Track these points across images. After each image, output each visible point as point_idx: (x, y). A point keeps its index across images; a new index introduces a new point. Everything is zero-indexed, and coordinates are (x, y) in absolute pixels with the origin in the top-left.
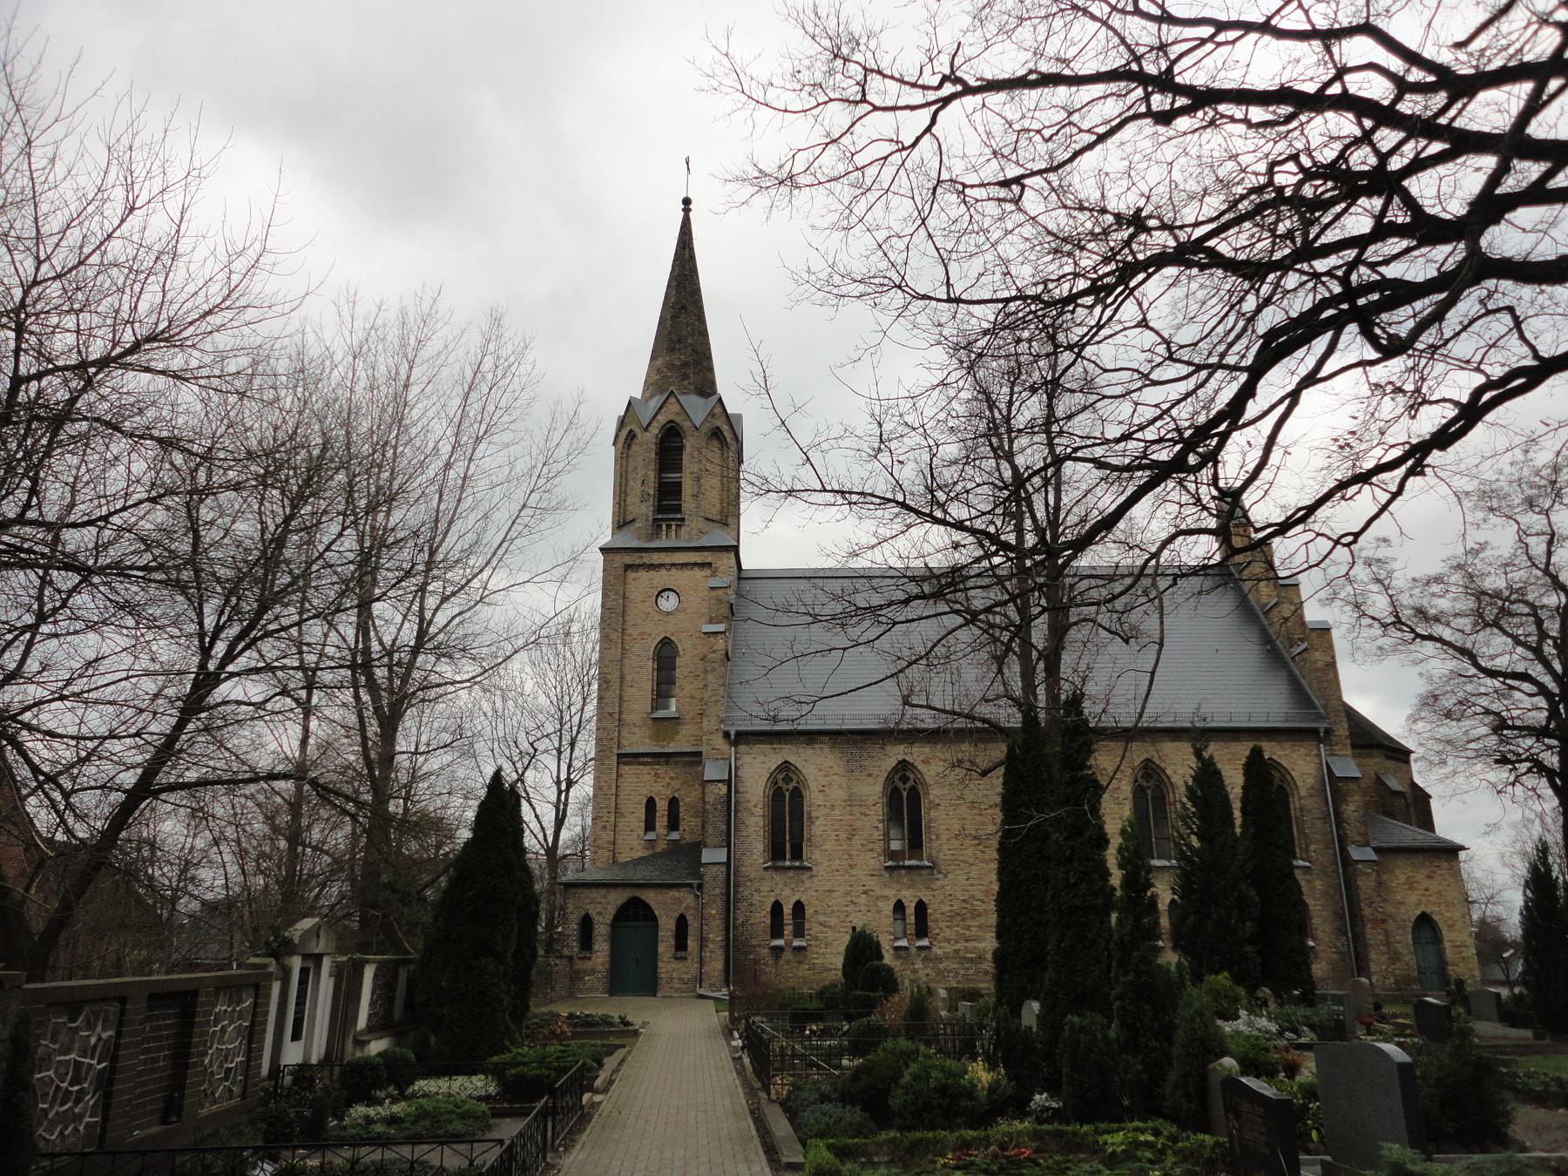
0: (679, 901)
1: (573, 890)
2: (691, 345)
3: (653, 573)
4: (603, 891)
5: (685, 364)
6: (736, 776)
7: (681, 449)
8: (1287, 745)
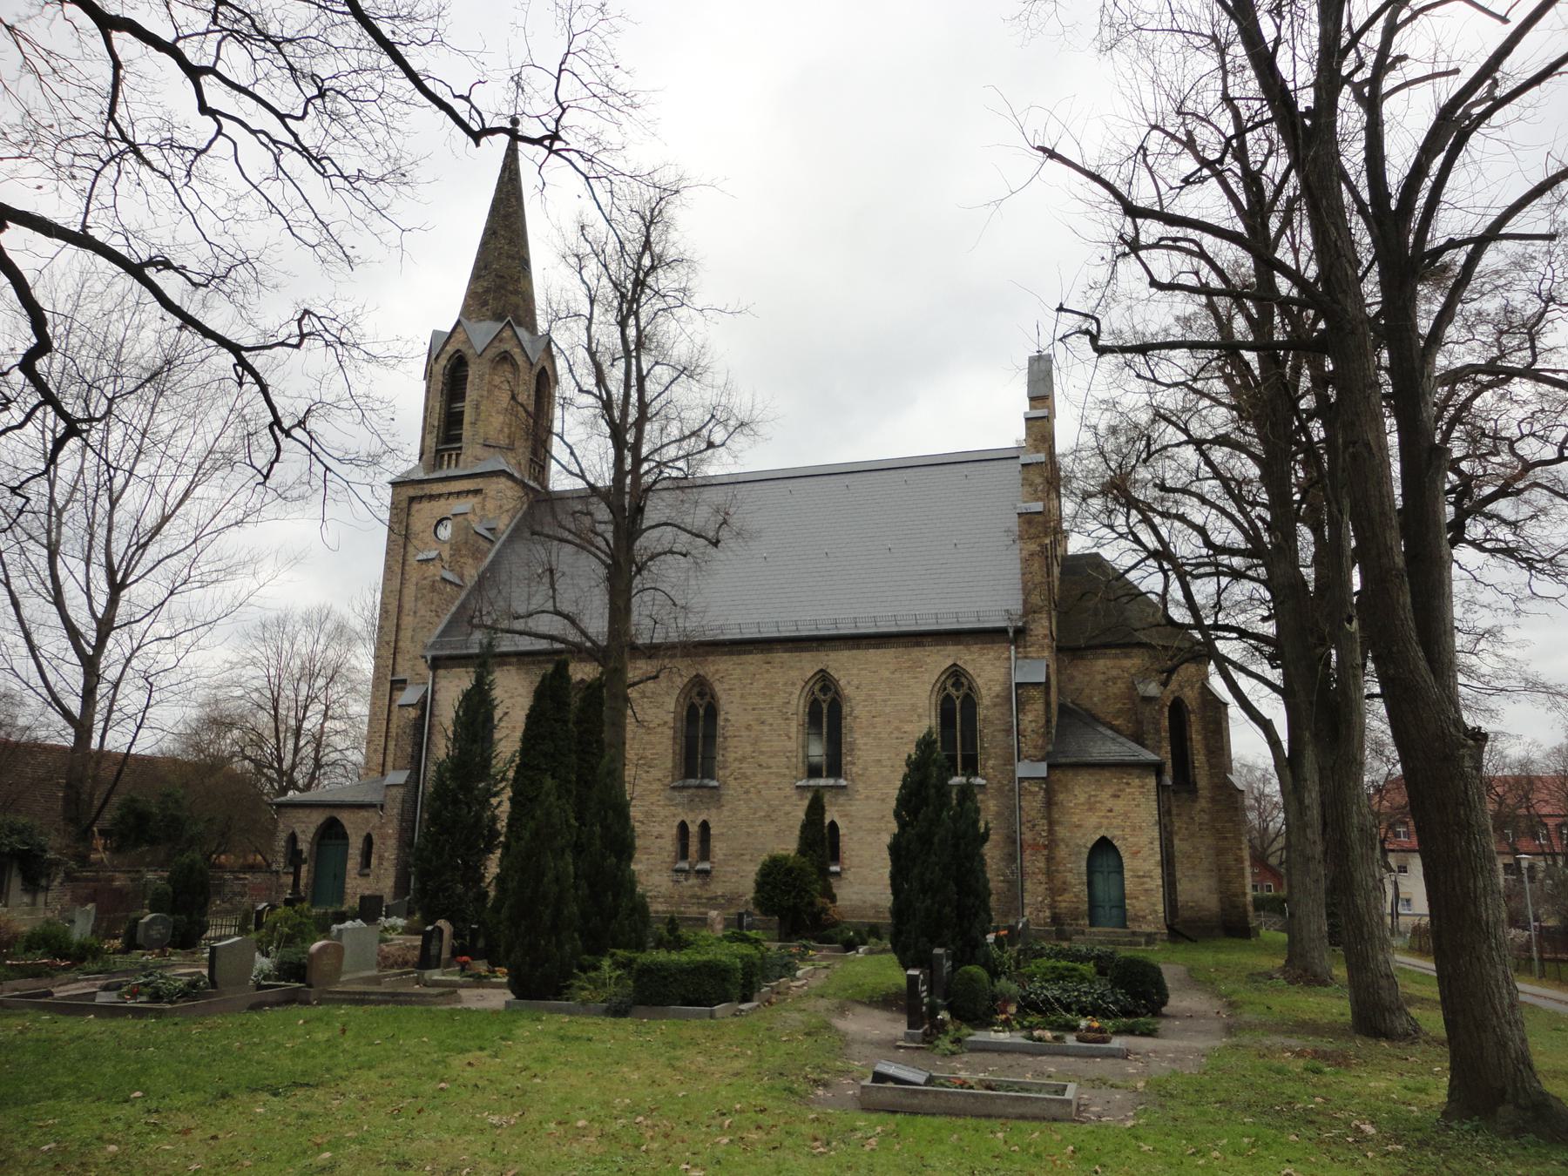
0: (367, 820)
1: (283, 810)
2: (495, 270)
3: (434, 503)
4: (308, 811)
5: (487, 291)
6: (433, 699)
7: (466, 377)
8: (975, 648)
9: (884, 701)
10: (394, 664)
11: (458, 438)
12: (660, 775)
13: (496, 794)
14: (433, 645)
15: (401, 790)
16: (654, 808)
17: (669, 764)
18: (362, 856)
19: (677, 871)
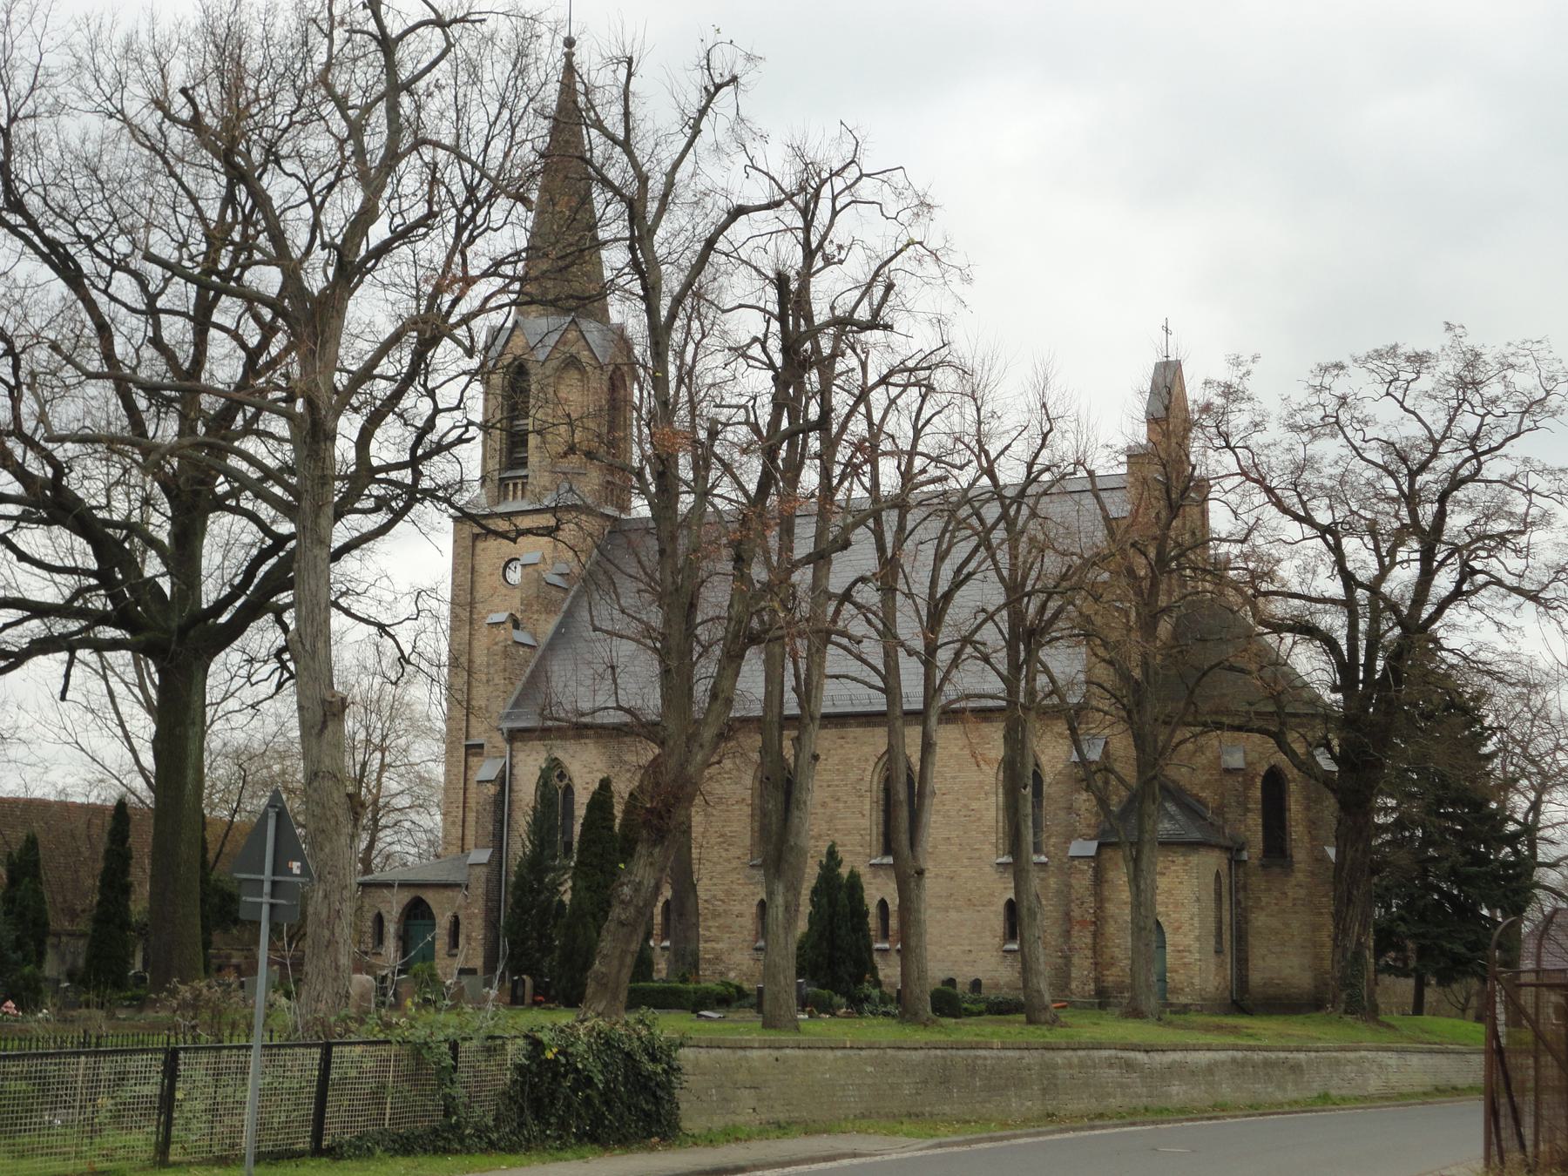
1: (367, 890)
6: (511, 773)
9: (954, 778)
10: (467, 727)
11: (523, 463)
12: (739, 853)
13: (561, 884)
14: (508, 716)
15: (485, 870)
16: (734, 886)
17: (748, 842)
18: (450, 936)
19: (757, 949)
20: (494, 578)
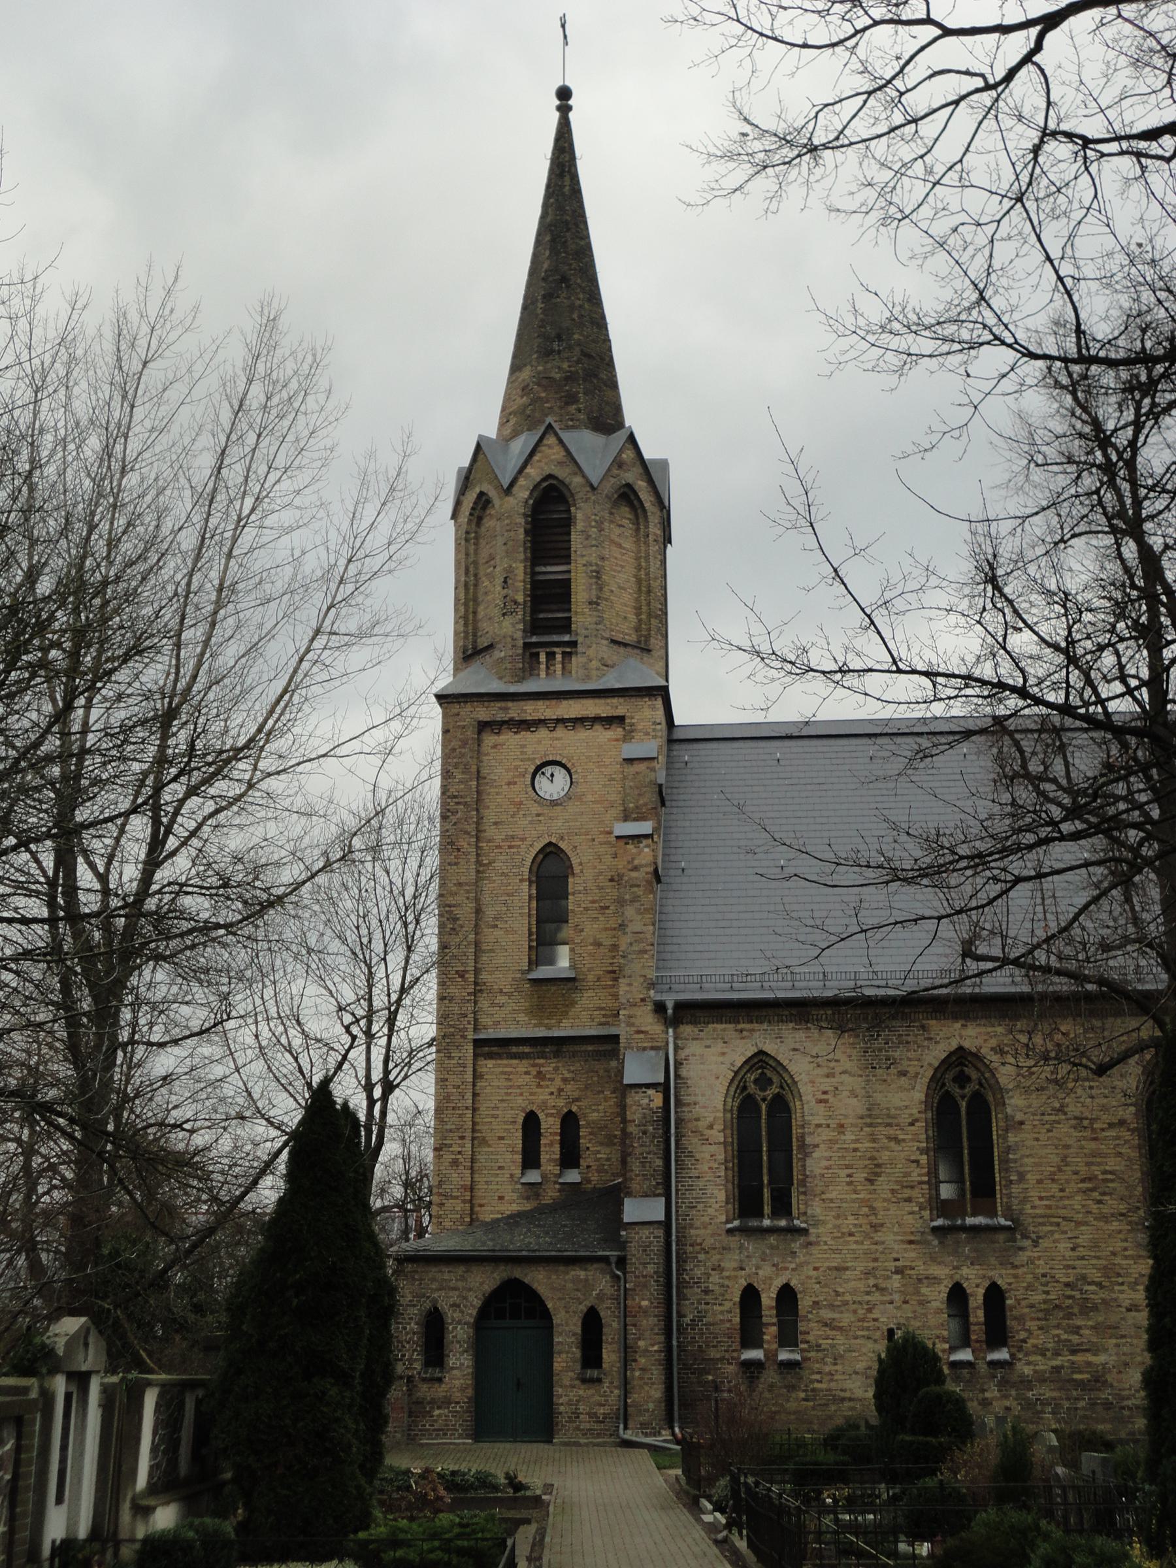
0: (587, 1285)
2: (579, 343)
4: (461, 1270)
5: (570, 378)
6: (677, 1076)
11: (565, 626)
16: (1118, 1260)
20: (515, 788)
